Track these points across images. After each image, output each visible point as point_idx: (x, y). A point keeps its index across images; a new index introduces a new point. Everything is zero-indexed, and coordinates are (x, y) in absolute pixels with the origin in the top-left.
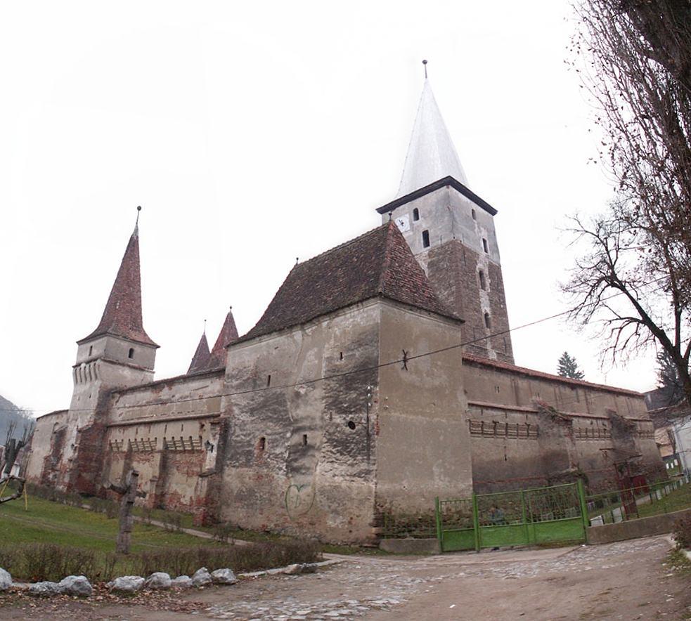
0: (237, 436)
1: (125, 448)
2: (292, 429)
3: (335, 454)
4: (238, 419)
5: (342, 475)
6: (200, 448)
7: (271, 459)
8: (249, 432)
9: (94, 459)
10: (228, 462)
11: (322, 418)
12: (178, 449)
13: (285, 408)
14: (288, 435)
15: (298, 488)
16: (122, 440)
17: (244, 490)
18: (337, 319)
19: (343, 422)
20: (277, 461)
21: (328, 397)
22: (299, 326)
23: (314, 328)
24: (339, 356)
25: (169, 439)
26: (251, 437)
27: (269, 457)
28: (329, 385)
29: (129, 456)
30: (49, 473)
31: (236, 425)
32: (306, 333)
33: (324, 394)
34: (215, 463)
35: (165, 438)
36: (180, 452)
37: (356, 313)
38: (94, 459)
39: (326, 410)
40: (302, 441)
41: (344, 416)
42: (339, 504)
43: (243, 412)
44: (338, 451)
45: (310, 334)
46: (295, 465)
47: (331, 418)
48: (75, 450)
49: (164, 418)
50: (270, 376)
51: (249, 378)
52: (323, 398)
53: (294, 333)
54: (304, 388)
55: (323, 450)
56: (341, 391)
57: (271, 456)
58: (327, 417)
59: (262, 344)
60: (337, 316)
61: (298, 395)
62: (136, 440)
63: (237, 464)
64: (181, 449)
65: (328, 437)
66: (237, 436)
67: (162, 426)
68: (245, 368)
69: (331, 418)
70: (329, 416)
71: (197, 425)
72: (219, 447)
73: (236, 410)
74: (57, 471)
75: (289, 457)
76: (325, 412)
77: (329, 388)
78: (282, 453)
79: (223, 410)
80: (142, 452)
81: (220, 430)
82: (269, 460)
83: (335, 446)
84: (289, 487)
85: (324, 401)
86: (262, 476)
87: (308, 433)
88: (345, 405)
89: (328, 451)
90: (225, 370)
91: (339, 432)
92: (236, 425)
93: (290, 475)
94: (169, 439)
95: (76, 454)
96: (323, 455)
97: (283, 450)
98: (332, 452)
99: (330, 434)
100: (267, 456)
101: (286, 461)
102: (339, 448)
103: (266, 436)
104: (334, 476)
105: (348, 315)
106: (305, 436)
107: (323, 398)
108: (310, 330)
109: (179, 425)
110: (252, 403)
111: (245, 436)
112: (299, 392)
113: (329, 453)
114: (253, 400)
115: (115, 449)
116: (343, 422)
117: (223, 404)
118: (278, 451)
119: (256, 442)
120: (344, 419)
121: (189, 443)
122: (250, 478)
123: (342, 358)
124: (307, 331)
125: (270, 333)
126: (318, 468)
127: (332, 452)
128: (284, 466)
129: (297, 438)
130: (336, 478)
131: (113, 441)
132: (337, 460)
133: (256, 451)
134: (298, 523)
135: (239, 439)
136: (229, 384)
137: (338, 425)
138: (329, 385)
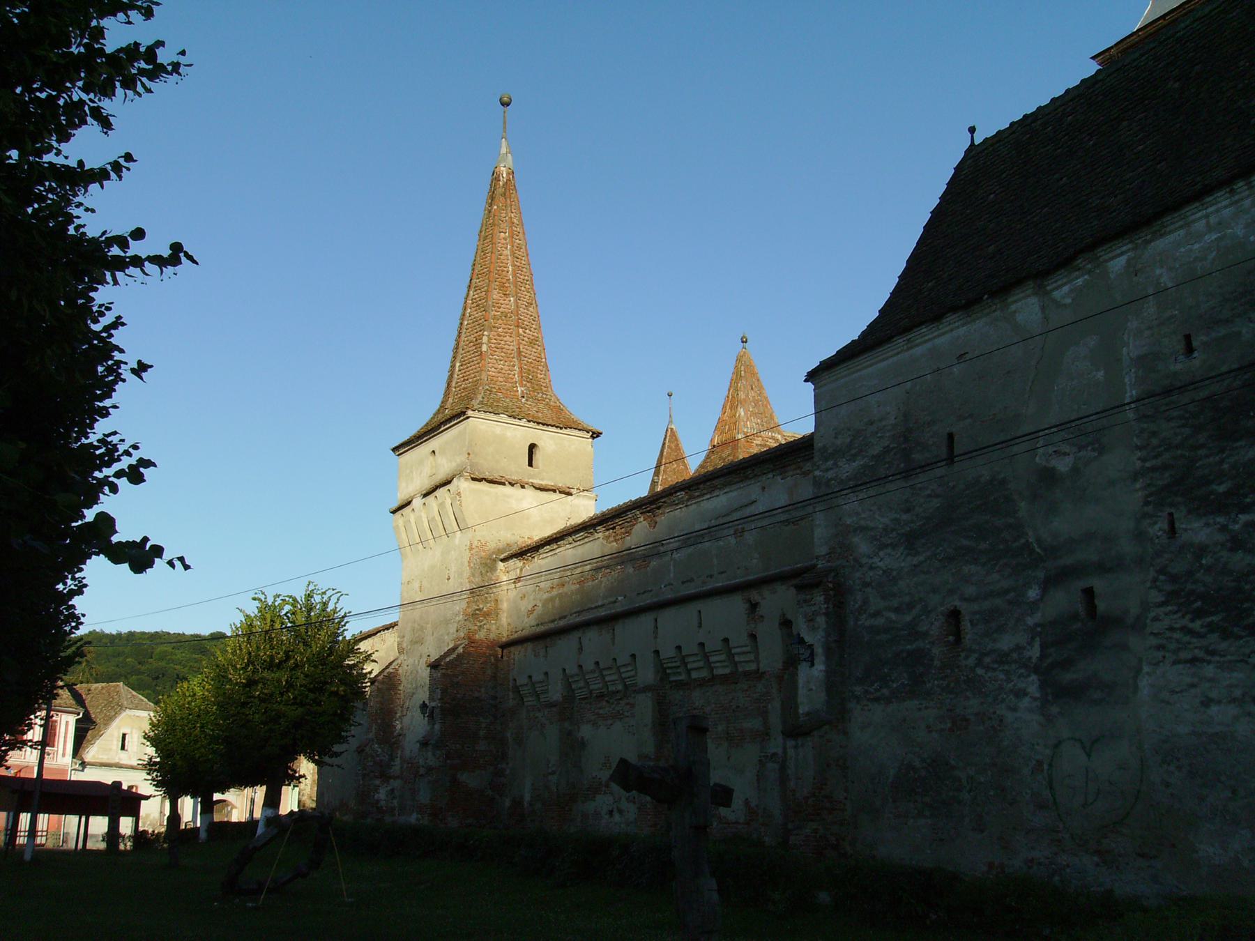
0: (877, 614)
1: (556, 692)
2: (1041, 574)
3: (1200, 636)
4: (871, 568)
5: (1234, 700)
6: (753, 667)
7: (987, 668)
8: (907, 599)
9: (482, 733)
10: (858, 690)
11: (1139, 536)
12: (694, 675)
13: (1011, 521)
14: (1033, 594)
15: (1084, 748)
16: (546, 674)
17: (917, 763)
18: (1160, 244)
19: (1220, 537)
20: (1007, 673)
21: (1153, 469)
22: (1031, 283)
23: (1080, 282)
24: (1181, 347)
25: (668, 652)
26: (914, 612)
27: (979, 663)
28: (1154, 434)
29: (567, 709)
30: (376, 790)
31: (867, 585)
32: (1054, 301)
33: (1138, 464)
34: (823, 694)
35: (657, 652)
36: (702, 683)
37: (1227, 212)
38: (482, 733)
39: (1149, 509)
40: (1081, 609)
41: (1221, 520)
42: (1234, 792)
43: (883, 547)
44: (1211, 628)
45: (1068, 301)
46: (1068, 677)
47: (1172, 531)
48: (431, 716)
49: (647, 600)
50: (951, 437)
51: (887, 450)
52: (1135, 476)
53: (1013, 307)
54: (1065, 454)
55: (1157, 626)
56: (1202, 446)
57: (987, 660)
58: (1160, 527)
59: (918, 351)
60: (1161, 235)
61: (1048, 477)
62: (580, 667)
63: (885, 691)
64: (704, 674)
65: (1169, 587)
66: (877, 614)
67: (647, 620)
68: (871, 423)
69: (1172, 531)
70: (1163, 524)
71: (737, 604)
72: (828, 651)
73: (862, 546)
74: (395, 778)
75: (1043, 657)
76: (1145, 515)
77: (1155, 441)
78: (1018, 648)
79: (822, 550)
80: (601, 696)
81: (826, 602)
82: (979, 671)
83: (1198, 614)
84: (1057, 746)
85: (1138, 486)
86: (967, 720)
87: (1098, 584)
88: (1222, 489)
89: (1171, 629)
90: (813, 445)
91: (1209, 569)
92: (867, 585)
93: (1054, 710)
94: (668, 652)
95: (437, 727)
96: (1154, 641)
97: (1021, 639)
98: (1191, 632)
99: (1174, 579)
100: (971, 661)
101: (1036, 670)
102: (1215, 618)
103: (963, 607)
104: (1207, 702)
105: (1200, 225)
106: (1089, 593)
107: (1135, 476)
108: (1066, 289)
109: (691, 610)
110: (905, 517)
111: (897, 610)
112: (1053, 469)
113: (1177, 635)
114: (908, 510)
115: (530, 701)
116: (1220, 537)
117: (819, 533)
118: (1006, 642)
119: (935, 626)
120: (1224, 528)
121: (723, 657)
122: (929, 729)
123: (1190, 350)
124: (1057, 295)
125: (937, 318)
126: (1144, 682)
127: (1191, 632)
128: (1032, 685)
129: (1063, 601)
130: (1214, 709)
131: (522, 680)
132: (1213, 653)
133: (936, 651)
134: (1098, 852)
135: (880, 621)
136: (830, 475)
137: (1202, 550)
138: (1154, 434)
